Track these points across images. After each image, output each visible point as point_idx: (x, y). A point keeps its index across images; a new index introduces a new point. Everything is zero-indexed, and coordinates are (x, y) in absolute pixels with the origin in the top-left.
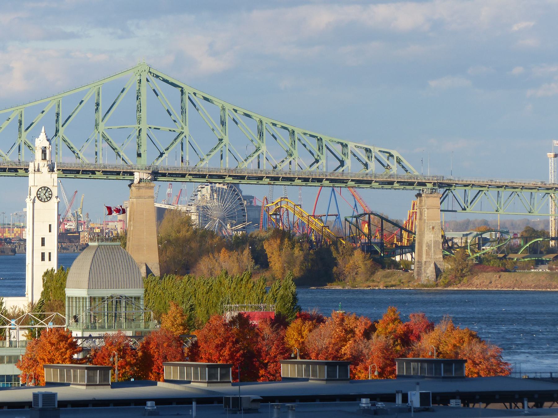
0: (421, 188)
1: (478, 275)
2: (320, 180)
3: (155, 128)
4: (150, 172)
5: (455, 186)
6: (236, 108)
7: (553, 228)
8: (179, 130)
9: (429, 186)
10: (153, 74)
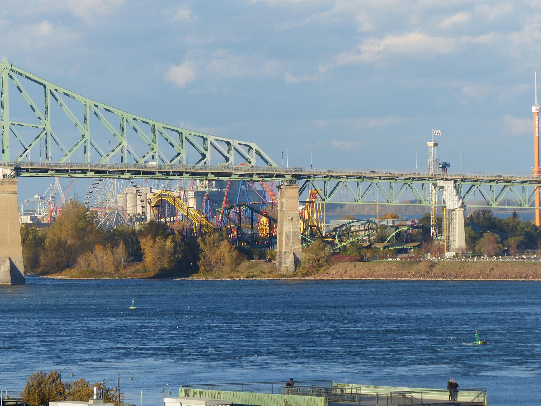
0: (280, 179)
1: (334, 264)
2: (181, 174)
3: (18, 125)
4: (13, 168)
5: (314, 178)
6: (97, 104)
7: (434, 216)
8: (41, 127)
9: (288, 178)
10: (17, 72)
